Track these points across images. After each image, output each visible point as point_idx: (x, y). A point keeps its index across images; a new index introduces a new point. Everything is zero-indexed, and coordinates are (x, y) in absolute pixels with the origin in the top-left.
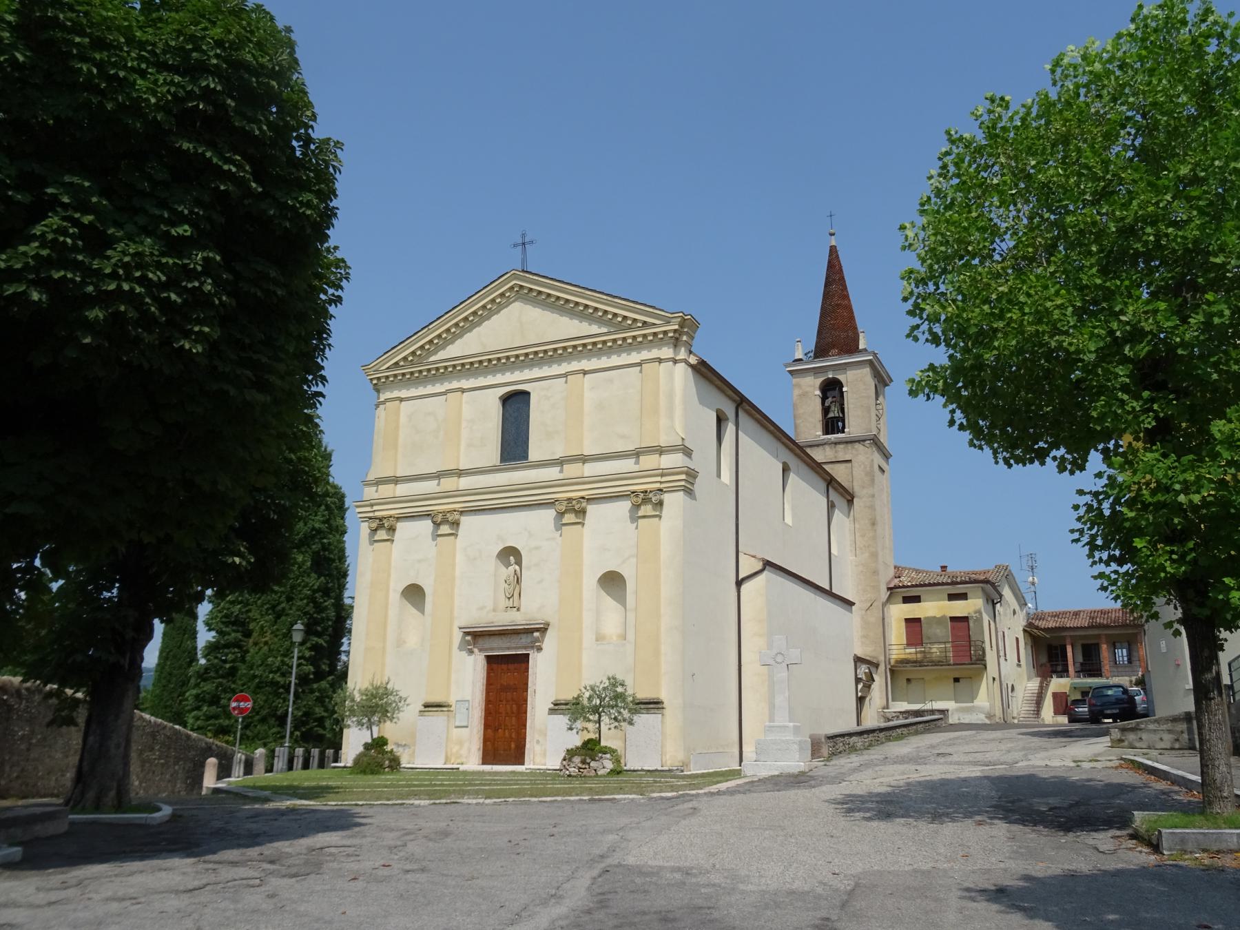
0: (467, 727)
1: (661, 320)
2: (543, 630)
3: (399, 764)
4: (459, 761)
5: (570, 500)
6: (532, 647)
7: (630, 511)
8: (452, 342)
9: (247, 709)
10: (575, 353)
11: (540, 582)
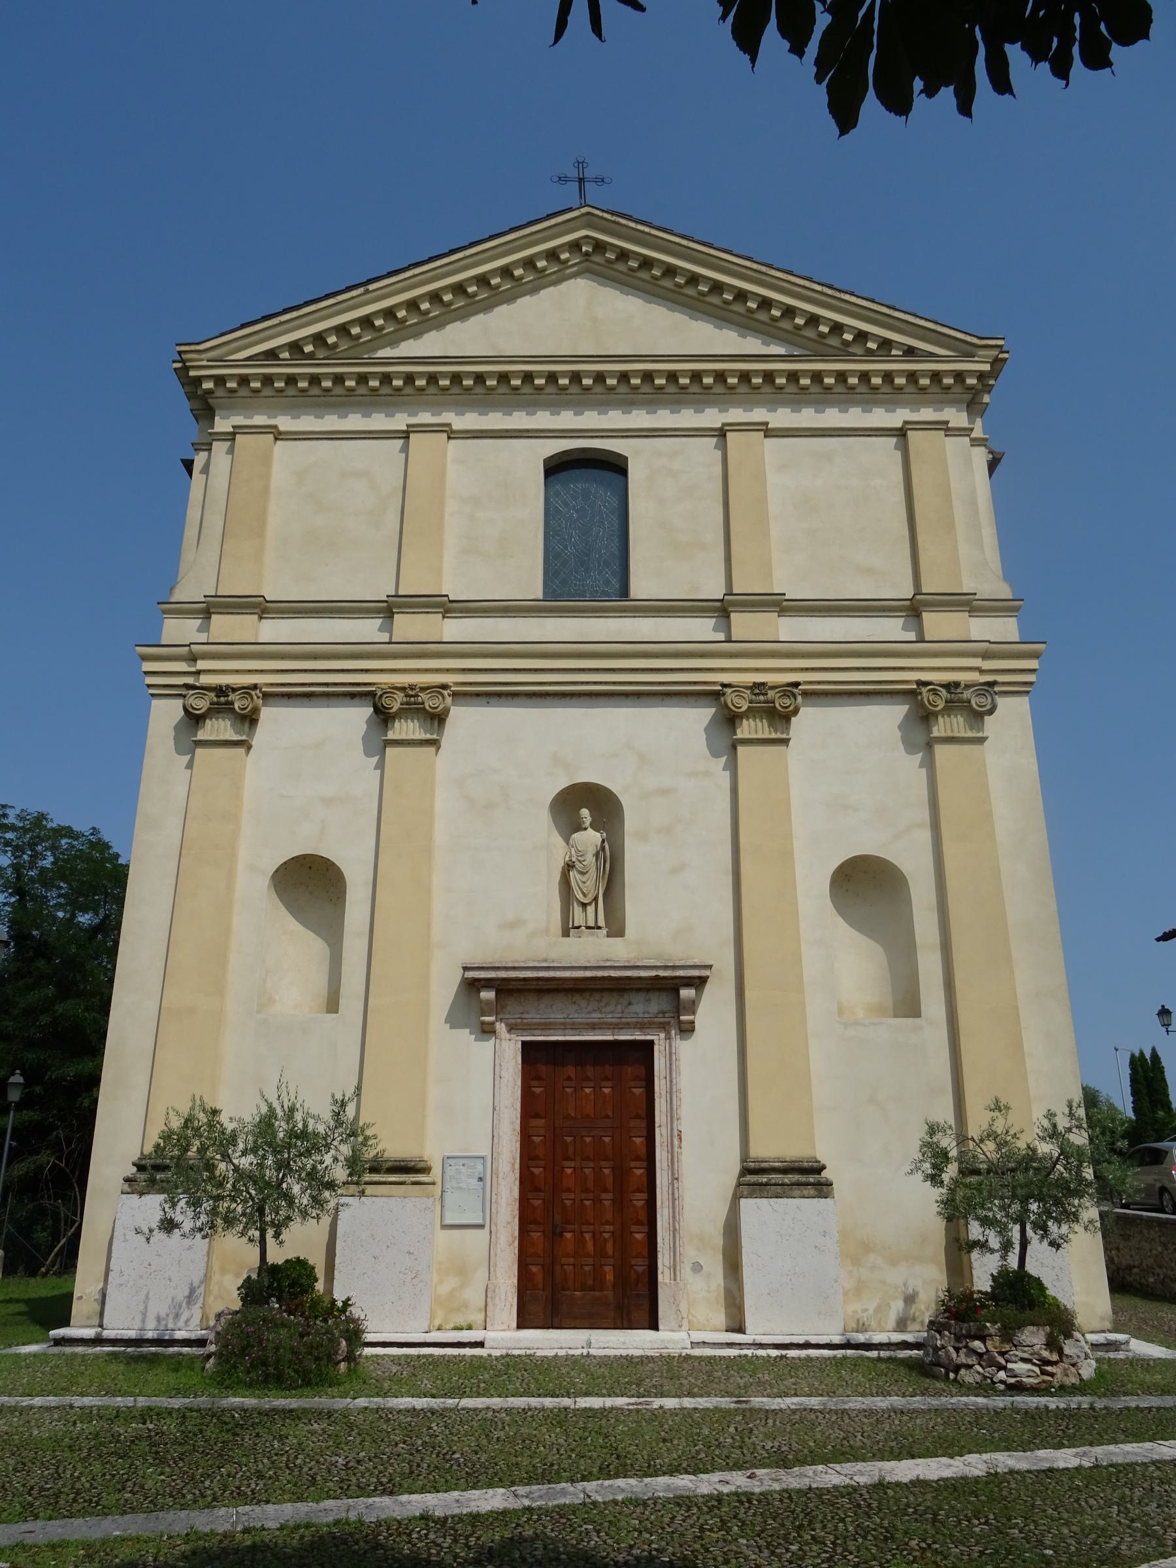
0: (482, 1226)
1: (948, 348)
2: (699, 983)
3: (355, 1335)
4: (460, 1320)
5: (758, 688)
6: (664, 1027)
10: (267, 392)
11: (675, 871)
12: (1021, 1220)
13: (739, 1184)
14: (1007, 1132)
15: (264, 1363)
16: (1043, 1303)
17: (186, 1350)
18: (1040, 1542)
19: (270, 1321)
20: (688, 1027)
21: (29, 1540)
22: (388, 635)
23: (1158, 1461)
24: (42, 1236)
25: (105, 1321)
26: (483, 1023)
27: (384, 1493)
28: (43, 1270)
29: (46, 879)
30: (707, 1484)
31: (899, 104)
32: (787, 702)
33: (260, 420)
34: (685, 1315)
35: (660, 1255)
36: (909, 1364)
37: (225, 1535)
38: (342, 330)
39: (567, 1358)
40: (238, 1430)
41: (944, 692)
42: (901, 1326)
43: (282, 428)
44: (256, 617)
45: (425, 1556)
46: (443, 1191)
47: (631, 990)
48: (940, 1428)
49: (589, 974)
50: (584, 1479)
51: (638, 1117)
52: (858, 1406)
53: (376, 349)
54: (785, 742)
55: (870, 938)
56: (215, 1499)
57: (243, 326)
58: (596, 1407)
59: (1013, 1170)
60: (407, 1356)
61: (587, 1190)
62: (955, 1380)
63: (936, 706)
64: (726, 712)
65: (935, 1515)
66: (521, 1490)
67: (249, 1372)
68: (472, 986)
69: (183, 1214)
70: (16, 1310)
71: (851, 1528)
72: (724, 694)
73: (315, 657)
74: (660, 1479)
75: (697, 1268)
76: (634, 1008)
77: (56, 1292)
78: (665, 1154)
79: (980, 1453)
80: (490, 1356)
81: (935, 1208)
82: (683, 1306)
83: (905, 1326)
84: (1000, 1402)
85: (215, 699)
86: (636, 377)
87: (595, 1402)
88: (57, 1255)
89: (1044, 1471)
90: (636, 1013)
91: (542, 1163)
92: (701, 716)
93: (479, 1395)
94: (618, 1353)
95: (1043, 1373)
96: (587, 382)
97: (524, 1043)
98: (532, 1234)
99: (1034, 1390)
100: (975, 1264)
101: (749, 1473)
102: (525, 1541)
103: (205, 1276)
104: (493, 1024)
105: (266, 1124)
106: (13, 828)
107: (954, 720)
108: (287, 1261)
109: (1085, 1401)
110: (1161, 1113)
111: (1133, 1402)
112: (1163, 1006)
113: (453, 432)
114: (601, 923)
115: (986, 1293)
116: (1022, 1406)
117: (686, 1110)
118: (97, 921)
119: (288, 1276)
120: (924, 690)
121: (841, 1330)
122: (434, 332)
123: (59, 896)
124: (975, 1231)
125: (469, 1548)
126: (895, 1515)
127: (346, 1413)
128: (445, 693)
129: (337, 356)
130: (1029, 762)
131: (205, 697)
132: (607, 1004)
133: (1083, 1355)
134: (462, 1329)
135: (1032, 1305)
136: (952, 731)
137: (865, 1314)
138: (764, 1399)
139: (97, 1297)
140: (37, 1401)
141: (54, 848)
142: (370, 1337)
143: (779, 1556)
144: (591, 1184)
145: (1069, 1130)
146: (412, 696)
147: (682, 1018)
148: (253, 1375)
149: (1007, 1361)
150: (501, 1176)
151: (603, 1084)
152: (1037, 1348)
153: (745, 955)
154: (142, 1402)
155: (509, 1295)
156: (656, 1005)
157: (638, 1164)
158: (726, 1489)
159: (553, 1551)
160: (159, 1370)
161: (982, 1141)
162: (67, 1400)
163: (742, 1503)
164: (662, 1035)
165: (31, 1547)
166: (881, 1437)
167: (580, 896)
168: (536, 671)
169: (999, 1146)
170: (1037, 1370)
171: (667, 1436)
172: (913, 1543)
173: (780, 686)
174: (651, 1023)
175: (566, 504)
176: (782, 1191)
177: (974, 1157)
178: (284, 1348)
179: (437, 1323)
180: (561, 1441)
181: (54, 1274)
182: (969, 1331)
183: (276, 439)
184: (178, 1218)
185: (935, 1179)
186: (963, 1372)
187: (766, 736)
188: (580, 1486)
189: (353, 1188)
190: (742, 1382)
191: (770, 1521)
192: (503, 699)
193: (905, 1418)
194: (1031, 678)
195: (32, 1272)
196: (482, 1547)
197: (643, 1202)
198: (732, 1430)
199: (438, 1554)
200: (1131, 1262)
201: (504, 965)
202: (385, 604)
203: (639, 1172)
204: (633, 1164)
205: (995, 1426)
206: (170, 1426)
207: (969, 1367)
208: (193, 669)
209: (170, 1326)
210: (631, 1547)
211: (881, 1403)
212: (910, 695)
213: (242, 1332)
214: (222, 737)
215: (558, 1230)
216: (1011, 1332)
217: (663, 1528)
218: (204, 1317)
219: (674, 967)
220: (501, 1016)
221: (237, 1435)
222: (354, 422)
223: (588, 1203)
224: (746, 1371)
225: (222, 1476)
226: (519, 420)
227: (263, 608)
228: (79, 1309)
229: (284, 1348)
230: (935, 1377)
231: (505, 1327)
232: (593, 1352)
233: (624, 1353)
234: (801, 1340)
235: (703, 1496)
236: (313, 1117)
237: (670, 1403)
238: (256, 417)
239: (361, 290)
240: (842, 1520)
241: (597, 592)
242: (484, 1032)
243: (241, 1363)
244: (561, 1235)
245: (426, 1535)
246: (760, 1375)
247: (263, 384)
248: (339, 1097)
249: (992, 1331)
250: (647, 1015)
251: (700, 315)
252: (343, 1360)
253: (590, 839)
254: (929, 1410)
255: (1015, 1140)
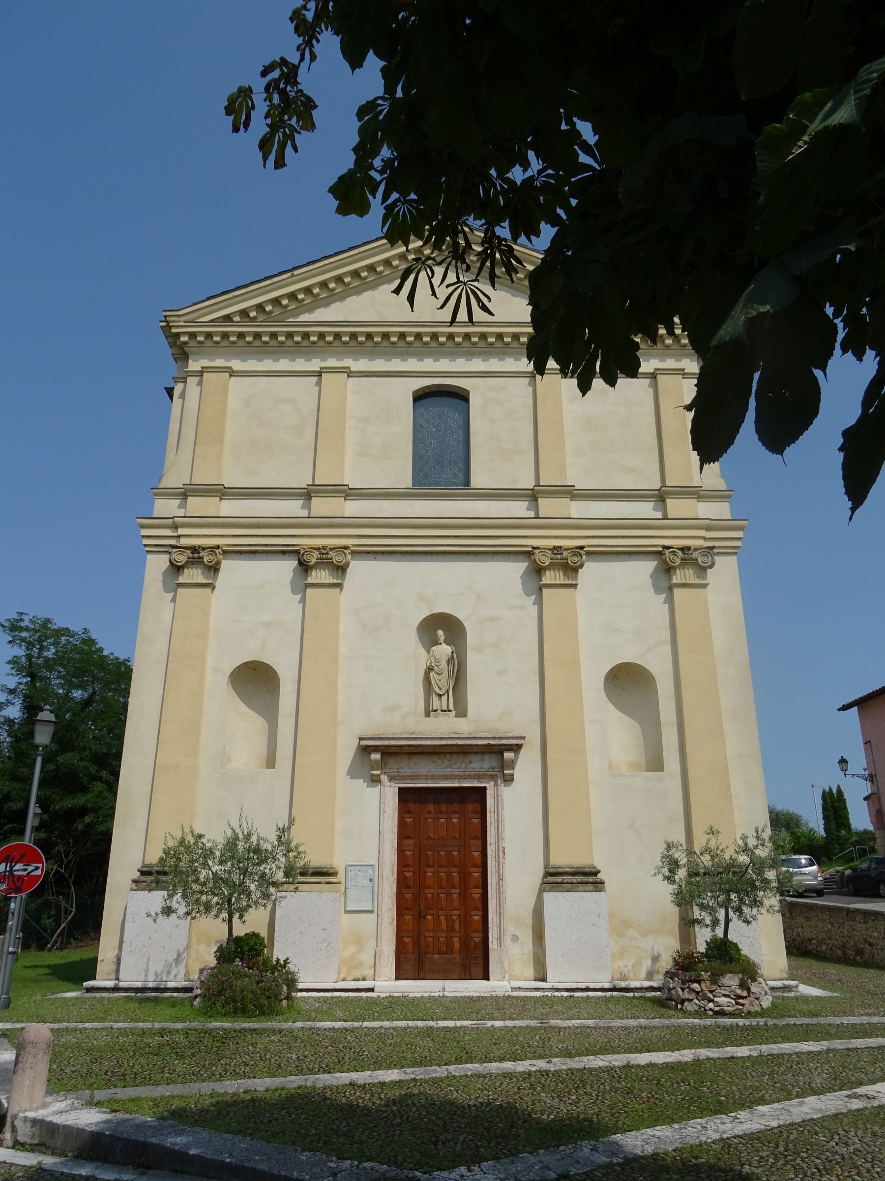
0: (371, 912)
3: (291, 982)
4: (358, 974)
5: (557, 549)
6: (493, 778)
7: (165, 574)
8: (342, 297)
9: (32, 879)
12: (726, 905)
13: (543, 883)
14: (718, 848)
15: (234, 1001)
16: (738, 959)
17: (175, 994)
18: (719, 1094)
19: (237, 974)
20: (509, 778)
21: (117, 1097)
22: (307, 511)
23: (799, 1053)
24: (48, 922)
25: (121, 976)
26: (372, 775)
27: (324, 1072)
28: (49, 946)
29: (49, 665)
30: (522, 1066)
31: (612, 382)
32: (576, 559)
33: (219, 362)
34: (507, 970)
35: (490, 931)
36: (653, 1000)
37: (234, 1094)
38: (276, 301)
39: (430, 997)
40: (224, 1040)
41: (680, 553)
42: (650, 976)
43: (234, 369)
44: (218, 498)
45: (355, 1103)
46: (345, 888)
47: (472, 753)
48: (668, 1036)
49: (443, 742)
50: (446, 1064)
51: (476, 838)
52: (618, 1024)
53: (298, 315)
54: (574, 586)
55: (631, 718)
56: (221, 1076)
57: (208, 299)
58: (451, 1026)
59: (721, 873)
60: (324, 997)
61: (442, 887)
62: (681, 1009)
63: (675, 563)
64: (535, 566)
65: (659, 1081)
66: (408, 1070)
67: (223, 1006)
68: (365, 750)
69: (179, 904)
70: (44, 973)
71: (608, 1088)
72: (534, 554)
73: (259, 526)
74: (493, 1064)
75: (515, 938)
76: (473, 765)
77: (63, 961)
78: (494, 863)
79: (691, 1049)
80: (379, 997)
81: (670, 898)
82: (506, 965)
83: (652, 976)
84: (708, 1022)
85: (191, 555)
86: (475, 336)
87: (451, 1024)
88: (58, 937)
89: (728, 1058)
90: (474, 768)
91: (412, 869)
92: (517, 568)
93: (374, 1020)
94: (463, 994)
95: (737, 1004)
96: (442, 339)
97: (400, 789)
98: (405, 916)
99: (731, 1015)
100: (698, 935)
101: (547, 1060)
102: (414, 1095)
103: (187, 945)
104: (379, 776)
105: (231, 845)
106: (27, 629)
107: (687, 572)
108: (246, 934)
109: (761, 1021)
110: (843, 832)
111: (792, 1021)
112: (842, 757)
113: (351, 372)
114: (451, 707)
115: (703, 953)
116: (722, 1024)
117: (508, 833)
118: (86, 695)
119: (247, 944)
120: (667, 552)
121: (609, 979)
122: (338, 303)
123: (58, 678)
124: (697, 913)
125: (381, 1099)
126: (635, 1081)
127: (290, 1031)
128: (347, 552)
129: (269, 320)
130: (736, 599)
131: (185, 554)
132: (456, 763)
133: (763, 993)
134: (359, 980)
135: (731, 961)
136: (686, 579)
137: (626, 969)
138: (558, 1021)
139: (114, 960)
140: (87, 1025)
141: (56, 644)
142: (301, 986)
143: (565, 1102)
144: (444, 883)
145: (756, 847)
146: (324, 554)
147: (505, 772)
148: (227, 1008)
149: (714, 996)
150: (384, 878)
151: (453, 816)
152: (733, 987)
153: (548, 730)
154: (157, 1025)
155: (390, 957)
156: (488, 763)
157: (476, 869)
158: (533, 1069)
159: (431, 1100)
160: (162, 1007)
161: (702, 854)
162: (107, 1024)
163: (543, 1076)
164: (492, 783)
165: (119, 1101)
166: (631, 1041)
167: (437, 690)
168: (407, 537)
169: (713, 859)
170: (733, 1002)
171: (496, 1042)
172: (644, 1095)
173: (572, 549)
174: (484, 775)
175: (427, 422)
176: (571, 887)
177: (697, 864)
178: (247, 991)
179: (342, 976)
180: (430, 1045)
181: (57, 949)
182: (690, 977)
183: (231, 376)
184: (174, 905)
185: (670, 879)
186: (686, 1003)
187: (562, 582)
188: (444, 1068)
189: (292, 887)
190: (544, 1012)
191: (560, 1085)
192: (385, 555)
193: (647, 1031)
194: (738, 543)
195: (42, 948)
196: (389, 1098)
197: (479, 895)
198: (537, 1038)
199: (363, 1102)
200: (810, 936)
201: (386, 736)
202: (306, 491)
203: (476, 875)
204: (472, 870)
205: (703, 1035)
206: (180, 1038)
207: (691, 1000)
208: (175, 534)
209: (164, 979)
210: (477, 1098)
211: (633, 1023)
212: (658, 554)
213: (218, 981)
214: (195, 581)
215: (422, 914)
216: (716, 977)
217: (496, 1089)
218: (187, 973)
219: (500, 738)
220: (384, 771)
221: (224, 1043)
222: (284, 364)
223: (442, 896)
224: (547, 1005)
225: (222, 1065)
226: (396, 365)
227: (222, 492)
228: (101, 968)
229: (247, 991)
230: (669, 1007)
231: (387, 978)
232: (446, 994)
233: (467, 995)
234: (583, 986)
235: (519, 1073)
236: (263, 839)
237: (498, 1024)
238: (217, 361)
239: (289, 275)
240: (603, 1084)
241: (448, 482)
242: (373, 781)
243: (218, 1001)
244: (424, 917)
245: (355, 1093)
246: (556, 1007)
247: (222, 338)
248: (281, 826)
249: (705, 977)
250: (482, 770)
251: (518, 293)
252: (285, 999)
253: (444, 650)
254: (663, 1026)
255: (722, 853)
